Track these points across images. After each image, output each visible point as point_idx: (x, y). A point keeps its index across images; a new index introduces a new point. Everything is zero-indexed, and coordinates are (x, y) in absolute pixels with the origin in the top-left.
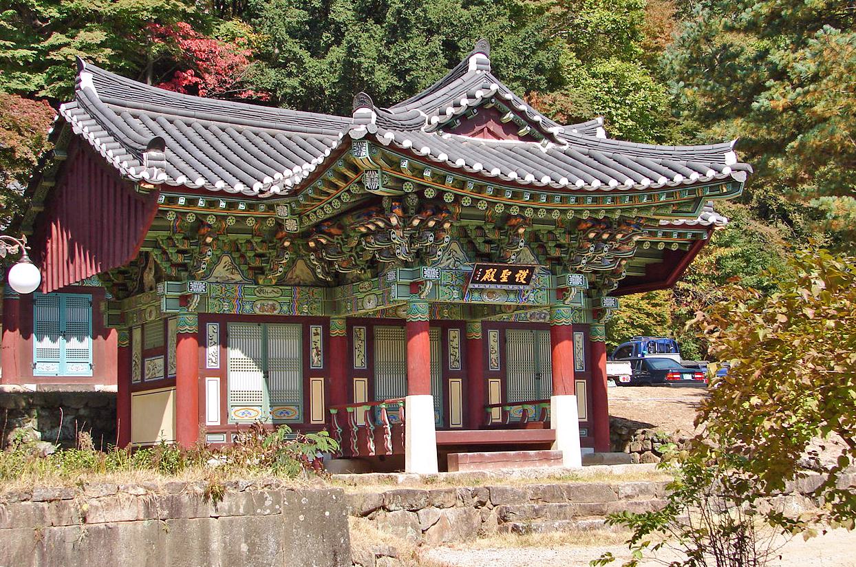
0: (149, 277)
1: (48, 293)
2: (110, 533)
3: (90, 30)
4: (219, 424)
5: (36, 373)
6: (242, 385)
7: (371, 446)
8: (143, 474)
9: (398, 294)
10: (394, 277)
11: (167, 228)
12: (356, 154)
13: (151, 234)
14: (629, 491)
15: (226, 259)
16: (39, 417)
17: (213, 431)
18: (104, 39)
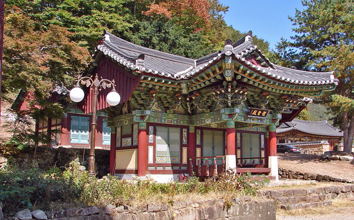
1: (105, 108)
3: (83, 41)
4: (152, 163)
5: (72, 142)
9: (225, 118)
10: (224, 111)
12: (226, 62)
14: (309, 192)
17: (151, 165)
18: (87, 43)
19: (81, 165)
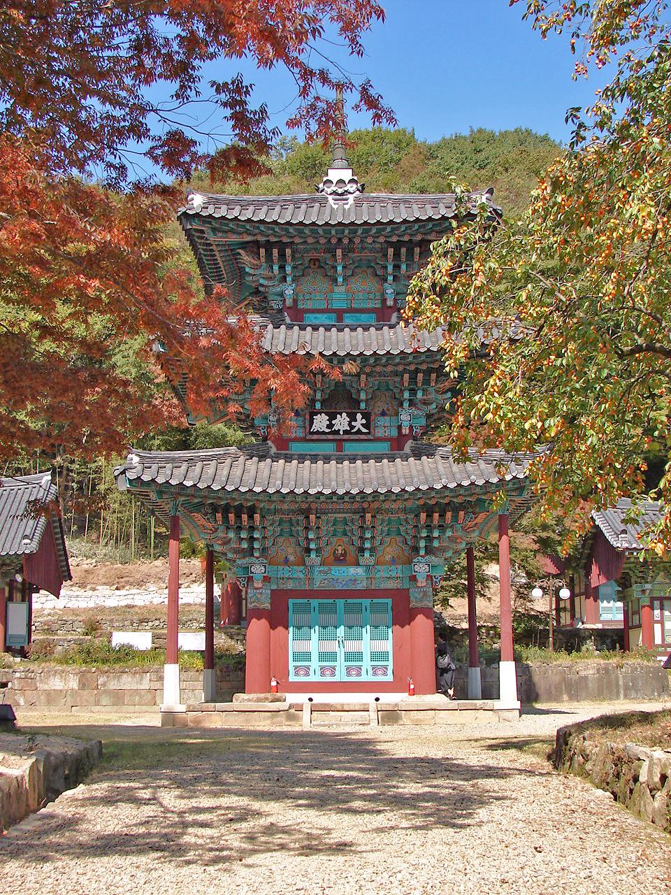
2: (586, 677)
5: (602, 619)
13: (625, 566)
15: (662, 573)
17: (658, 646)
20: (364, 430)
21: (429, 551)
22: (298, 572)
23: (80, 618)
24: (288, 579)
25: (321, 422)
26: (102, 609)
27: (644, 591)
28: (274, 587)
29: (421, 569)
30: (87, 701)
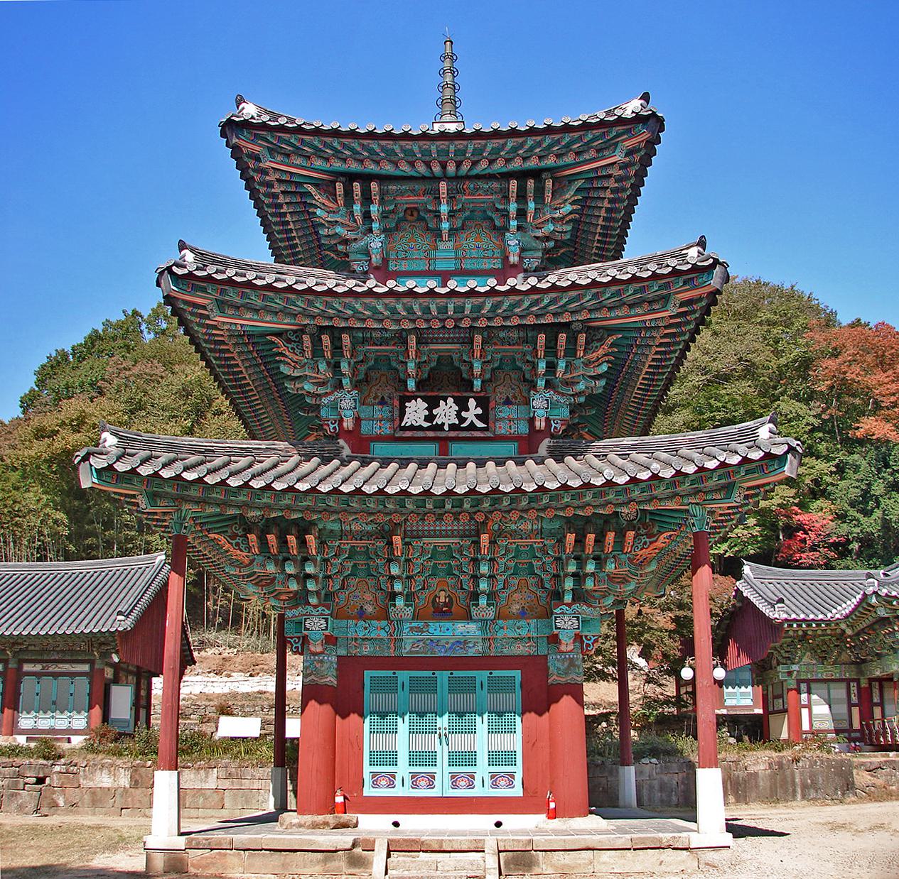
0: (774, 662)
2: (756, 774)
6: (818, 712)
7: (882, 739)
8: (767, 752)
11: (791, 637)
13: (772, 645)
16: (728, 726)
17: (806, 733)
19: (730, 736)
20: (480, 424)
21: (579, 596)
22: (378, 630)
23: (212, 703)
24: (363, 639)
25: (416, 412)
26: (234, 695)
27: (790, 673)
28: (342, 652)
29: (566, 624)
30: (140, 802)
